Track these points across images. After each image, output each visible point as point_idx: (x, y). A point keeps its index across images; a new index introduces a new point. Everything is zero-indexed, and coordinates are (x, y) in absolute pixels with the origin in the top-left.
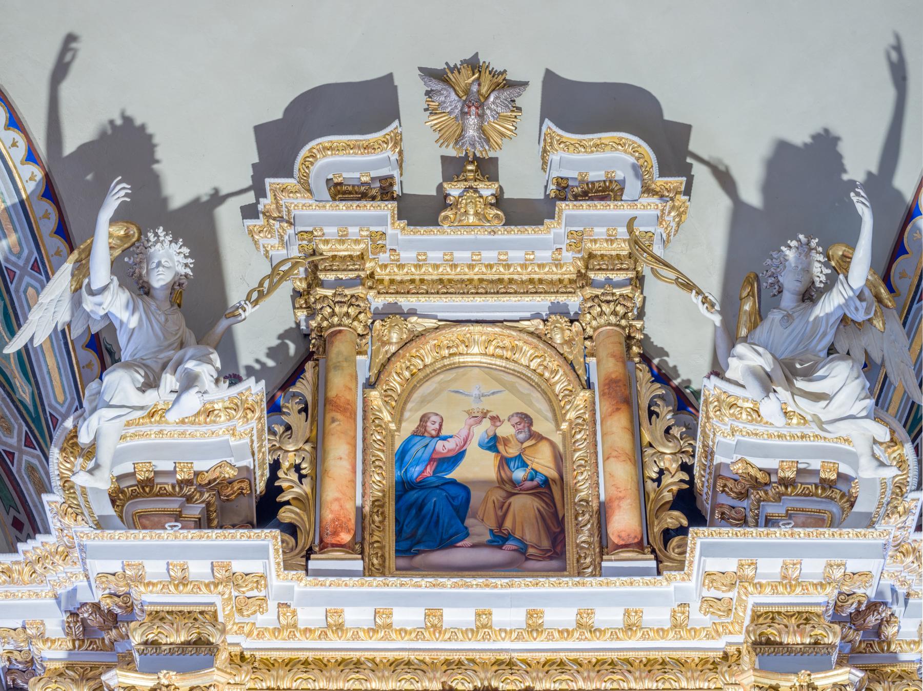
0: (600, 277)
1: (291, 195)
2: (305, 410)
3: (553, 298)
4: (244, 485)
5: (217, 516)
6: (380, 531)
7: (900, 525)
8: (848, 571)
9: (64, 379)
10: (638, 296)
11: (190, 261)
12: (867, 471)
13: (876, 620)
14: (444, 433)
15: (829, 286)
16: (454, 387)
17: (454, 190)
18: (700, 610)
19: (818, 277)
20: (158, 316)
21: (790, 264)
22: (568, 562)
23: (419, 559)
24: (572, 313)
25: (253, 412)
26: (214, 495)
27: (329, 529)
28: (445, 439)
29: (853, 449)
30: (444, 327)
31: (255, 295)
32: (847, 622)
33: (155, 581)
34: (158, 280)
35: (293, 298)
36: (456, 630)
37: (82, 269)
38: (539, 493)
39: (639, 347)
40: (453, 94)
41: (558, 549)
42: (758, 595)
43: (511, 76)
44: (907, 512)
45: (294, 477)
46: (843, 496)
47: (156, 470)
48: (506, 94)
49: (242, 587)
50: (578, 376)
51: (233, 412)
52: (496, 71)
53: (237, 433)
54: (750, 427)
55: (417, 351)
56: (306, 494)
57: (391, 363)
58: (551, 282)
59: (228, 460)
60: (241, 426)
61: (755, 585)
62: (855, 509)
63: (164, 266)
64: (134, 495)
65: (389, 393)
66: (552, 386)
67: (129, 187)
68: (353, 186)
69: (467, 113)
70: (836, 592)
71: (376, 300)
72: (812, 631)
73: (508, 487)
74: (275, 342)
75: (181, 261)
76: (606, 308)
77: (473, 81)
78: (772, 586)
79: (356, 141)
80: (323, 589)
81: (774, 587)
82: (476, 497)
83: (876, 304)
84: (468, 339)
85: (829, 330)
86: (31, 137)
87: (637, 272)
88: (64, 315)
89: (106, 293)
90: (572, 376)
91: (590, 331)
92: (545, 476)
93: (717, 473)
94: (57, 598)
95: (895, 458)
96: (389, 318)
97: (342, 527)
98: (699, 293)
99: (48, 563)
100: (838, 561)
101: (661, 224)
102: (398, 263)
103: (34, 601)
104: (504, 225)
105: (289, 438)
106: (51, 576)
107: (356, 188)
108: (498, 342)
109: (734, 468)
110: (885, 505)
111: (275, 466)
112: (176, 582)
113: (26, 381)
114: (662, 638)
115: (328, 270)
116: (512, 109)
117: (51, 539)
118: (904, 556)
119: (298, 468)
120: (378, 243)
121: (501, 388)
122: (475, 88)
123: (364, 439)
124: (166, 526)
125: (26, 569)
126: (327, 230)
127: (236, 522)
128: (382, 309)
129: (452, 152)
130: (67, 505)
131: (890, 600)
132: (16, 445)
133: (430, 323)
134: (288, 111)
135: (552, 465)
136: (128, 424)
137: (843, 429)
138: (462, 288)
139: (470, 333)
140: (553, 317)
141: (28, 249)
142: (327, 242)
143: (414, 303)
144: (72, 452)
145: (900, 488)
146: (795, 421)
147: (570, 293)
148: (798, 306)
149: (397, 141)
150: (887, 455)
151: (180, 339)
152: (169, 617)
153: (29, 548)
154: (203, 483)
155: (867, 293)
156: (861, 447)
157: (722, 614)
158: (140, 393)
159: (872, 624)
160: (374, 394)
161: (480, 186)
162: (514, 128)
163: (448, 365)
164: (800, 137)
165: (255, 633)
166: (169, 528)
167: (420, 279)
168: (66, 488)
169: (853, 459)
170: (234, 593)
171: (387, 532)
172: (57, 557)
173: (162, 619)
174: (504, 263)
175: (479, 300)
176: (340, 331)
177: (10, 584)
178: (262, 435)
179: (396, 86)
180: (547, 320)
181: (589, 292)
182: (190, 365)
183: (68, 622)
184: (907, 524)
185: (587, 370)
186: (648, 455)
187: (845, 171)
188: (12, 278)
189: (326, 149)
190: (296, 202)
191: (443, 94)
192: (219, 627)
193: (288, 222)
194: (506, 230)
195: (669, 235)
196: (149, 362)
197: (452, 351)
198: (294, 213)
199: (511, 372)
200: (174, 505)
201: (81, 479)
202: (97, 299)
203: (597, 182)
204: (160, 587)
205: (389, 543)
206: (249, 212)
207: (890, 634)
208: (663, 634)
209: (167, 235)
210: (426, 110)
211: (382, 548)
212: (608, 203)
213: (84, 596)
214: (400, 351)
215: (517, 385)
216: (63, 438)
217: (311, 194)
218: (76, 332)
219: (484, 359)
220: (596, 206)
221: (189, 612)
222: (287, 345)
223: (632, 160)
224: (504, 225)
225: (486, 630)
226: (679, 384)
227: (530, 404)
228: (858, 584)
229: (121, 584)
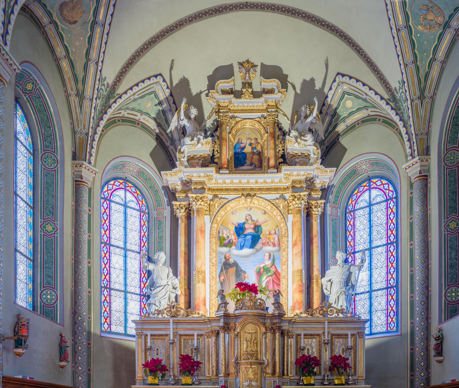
0: (270, 110)
2: (218, 138)
3: (262, 113)
11: (198, 112)
12: (312, 155)
14: (242, 142)
15: (310, 115)
16: (244, 132)
17: (244, 90)
23: (238, 168)
28: (242, 143)
43: (255, 64)
44: (318, 163)
45: (217, 153)
58: (261, 110)
64: (191, 159)
66: (261, 132)
74: (212, 122)
76: (271, 117)
88: (176, 124)
90: (265, 131)
93: (288, 153)
94: (179, 178)
98: (287, 117)
106: (178, 175)
111: (214, 150)
117: (178, 169)
122: (248, 68)
133: (240, 119)
134: (213, 72)
137: (309, 148)
141: (169, 107)
142: (221, 103)
153: (174, 170)
160: (230, 135)
164: (308, 79)
185: (267, 129)
187: (315, 87)
202: (182, 121)
227: (257, 136)
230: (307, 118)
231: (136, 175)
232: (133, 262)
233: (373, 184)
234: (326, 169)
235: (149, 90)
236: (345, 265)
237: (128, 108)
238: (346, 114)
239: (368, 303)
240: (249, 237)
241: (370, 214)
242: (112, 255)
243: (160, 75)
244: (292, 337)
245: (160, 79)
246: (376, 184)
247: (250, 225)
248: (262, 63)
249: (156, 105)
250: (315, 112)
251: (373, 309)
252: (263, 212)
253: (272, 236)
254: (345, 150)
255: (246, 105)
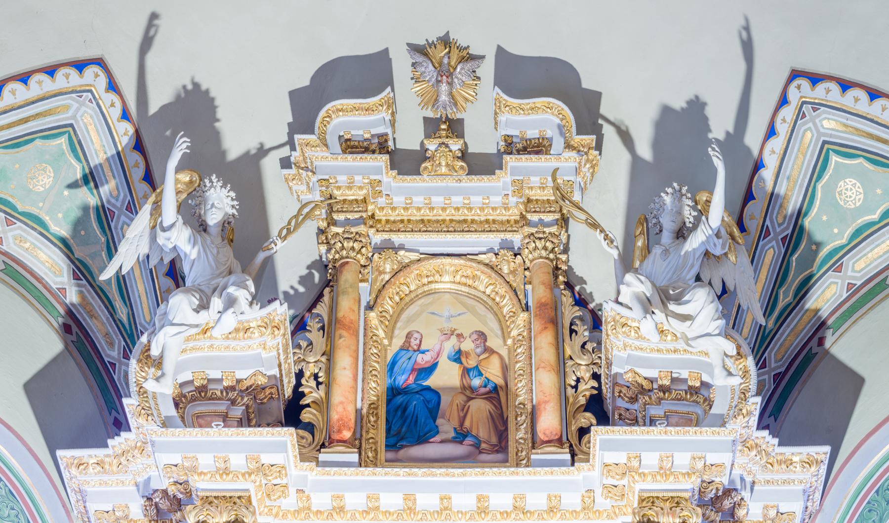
0: (534, 218)
1: (313, 149)
2: (323, 328)
3: (502, 236)
4: (274, 390)
5: (255, 417)
6: (374, 429)
7: (744, 425)
8: (708, 463)
9: (150, 302)
10: (564, 234)
11: (235, 203)
12: (719, 380)
13: (730, 503)
14: (423, 348)
15: (695, 226)
18: (602, 495)
19: (688, 218)
20: (211, 249)
21: (667, 209)
22: (510, 455)
23: (402, 453)
24: (516, 248)
25: (278, 329)
26: (251, 398)
27: (336, 428)
28: (423, 352)
29: (709, 360)
30: (424, 259)
31: (284, 232)
32: (709, 505)
33: (205, 471)
34: (212, 219)
35: (318, 235)
36: (426, 512)
37: (157, 208)
38: (490, 397)
39: (564, 277)
40: (431, 65)
41: (503, 444)
42: (642, 483)
44: (749, 413)
45: (313, 383)
46: (705, 400)
47: (209, 378)
48: (469, 65)
49: (268, 476)
50: (519, 300)
51: (264, 329)
52: (462, 46)
53: (267, 347)
54: (637, 343)
55: (404, 279)
56: (321, 398)
57: (385, 289)
58: (502, 223)
59: (260, 369)
60: (271, 342)
61: (640, 474)
62: (713, 411)
63: (216, 208)
64: (193, 399)
65: (384, 314)
67: (189, 140)
68: (359, 141)
69: (440, 81)
70: (699, 480)
71: (376, 236)
72: (681, 512)
73: (468, 393)
74: (304, 272)
75: (229, 203)
76: (540, 244)
77: (445, 55)
78: (652, 475)
79: (360, 104)
80: (329, 478)
81: (654, 476)
82: (445, 400)
83: (730, 241)
84: (441, 269)
85: (695, 262)
86: (125, 99)
87: (563, 215)
88: (144, 249)
89: (173, 229)
90: (515, 301)
91: (528, 264)
92: (496, 384)
94: (137, 485)
95: (741, 368)
96: (384, 252)
97: (344, 426)
98: (602, 231)
99: (130, 457)
100: (699, 454)
101: (579, 174)
102: (392, 206)
103: (120, 488)
104: (467, 175)
105: (310, 352)
106: (133, 467)
107: (361, 143)
108: (463, 272)
109: (626, 377)
110: (733, 408)
111: (300, 375)
112: (221, 472)
113: (123, 304)
114: (576, 519)
115: (340, 211)
116: (473, 78)
118: (749, 450)
119: (316, 377)
120: (376, 189)
121: (465, 310)
122: (446, 61)
123: (364, 352)
124: (213, 425)
125: (115, 461)
126: (339, 178)
127: (270, 421)
128: (380, 244)
129: (430, 114)
130: (141, 408)
131: (739, 487)
132: (116, 357)
133: (414, 256)
134: (313, 79)
135: (500, 374)
136: (188, 339)
137: (703, 344)
138: (438, 228)
139: (443, 265)
140: (502, 251)
141: (124, 192)
142: (339, 188)
143: (403, 239)
144: (146, 363)
145: (744, 393)
146: (669, 338)
147: (515, 231)
148: (673, 242)
149: (391, 104)
150: (735, 366)
151: (229, 268)
152: (216, 501)
153: (118, 443)
154: (243, 389)
155: (723, 232)
156: (715, 360)
157: (618, 498)
158: (195, 314)
159: (727, 507)
160: (372, 315)
161: (450, 142)
162: (475, 94)
163: (427, 291)
164: (678, 103)
165: (281, 514)
166: (215, 427)
167: (408, 220)
168: (141, 393)
169: (709, 368)
170: (264, 482)
171: (380, 430)
172: (136, 451)
173: (210, 503)
174: (468, 206)
175: (450, 237)
176: (347, 263)
177: (103, 474)
178: (288, 349)
179: (391, 59)
180: (498, 254)
181: (528, 230)
182: (231, 290)
183: (145, 505)
184: (750, 424)
185: (526, 296)
186: (569, 366)
187: (710, 131)
188: (112, 216)
189: (339, 110)
190: (316, 154)
191: (423, 66)
192: (251, 510)
193: (312, 171)
194: (468, 179)
195: (585, 183)
196: (203, 288)
197: (430, 279)
198: (315, 163)
199: (472, 297)
200: (222, 407)
201: (150, 386)
202: (167, 234)
203: (533, 139)
204: (209, 476)
205: (381, 439)
206: (286, 163)
207: (741, 515)
208: (576, 516)
209: (219, 181)
210: (412, 79)
211: (375, 443)
212: (540, 156)
213: (154, 485)
214: (392, 279)
215: (477, 308)
216: (140, 351)
217: (327, 148)
218: (153, 262)
219: (453, 286)
220: (532, 159)
221: (230, 497)
222: (313, 274)
223: (558, 121)
224: (467, 175)
225: (448, 512)
226: (594, 307)
227: (485, 324)
228: (715, 473)
229: (181, 474)
230: (685, 238)
234: (788, 450)
235: (48, 119)
238: (841, 234)
243: (99, 62)
245: (93, 77)
248: (500, 49)
249: (73, 186)
250: (717, 214)
254: (856, 382)
255: (437, 200)
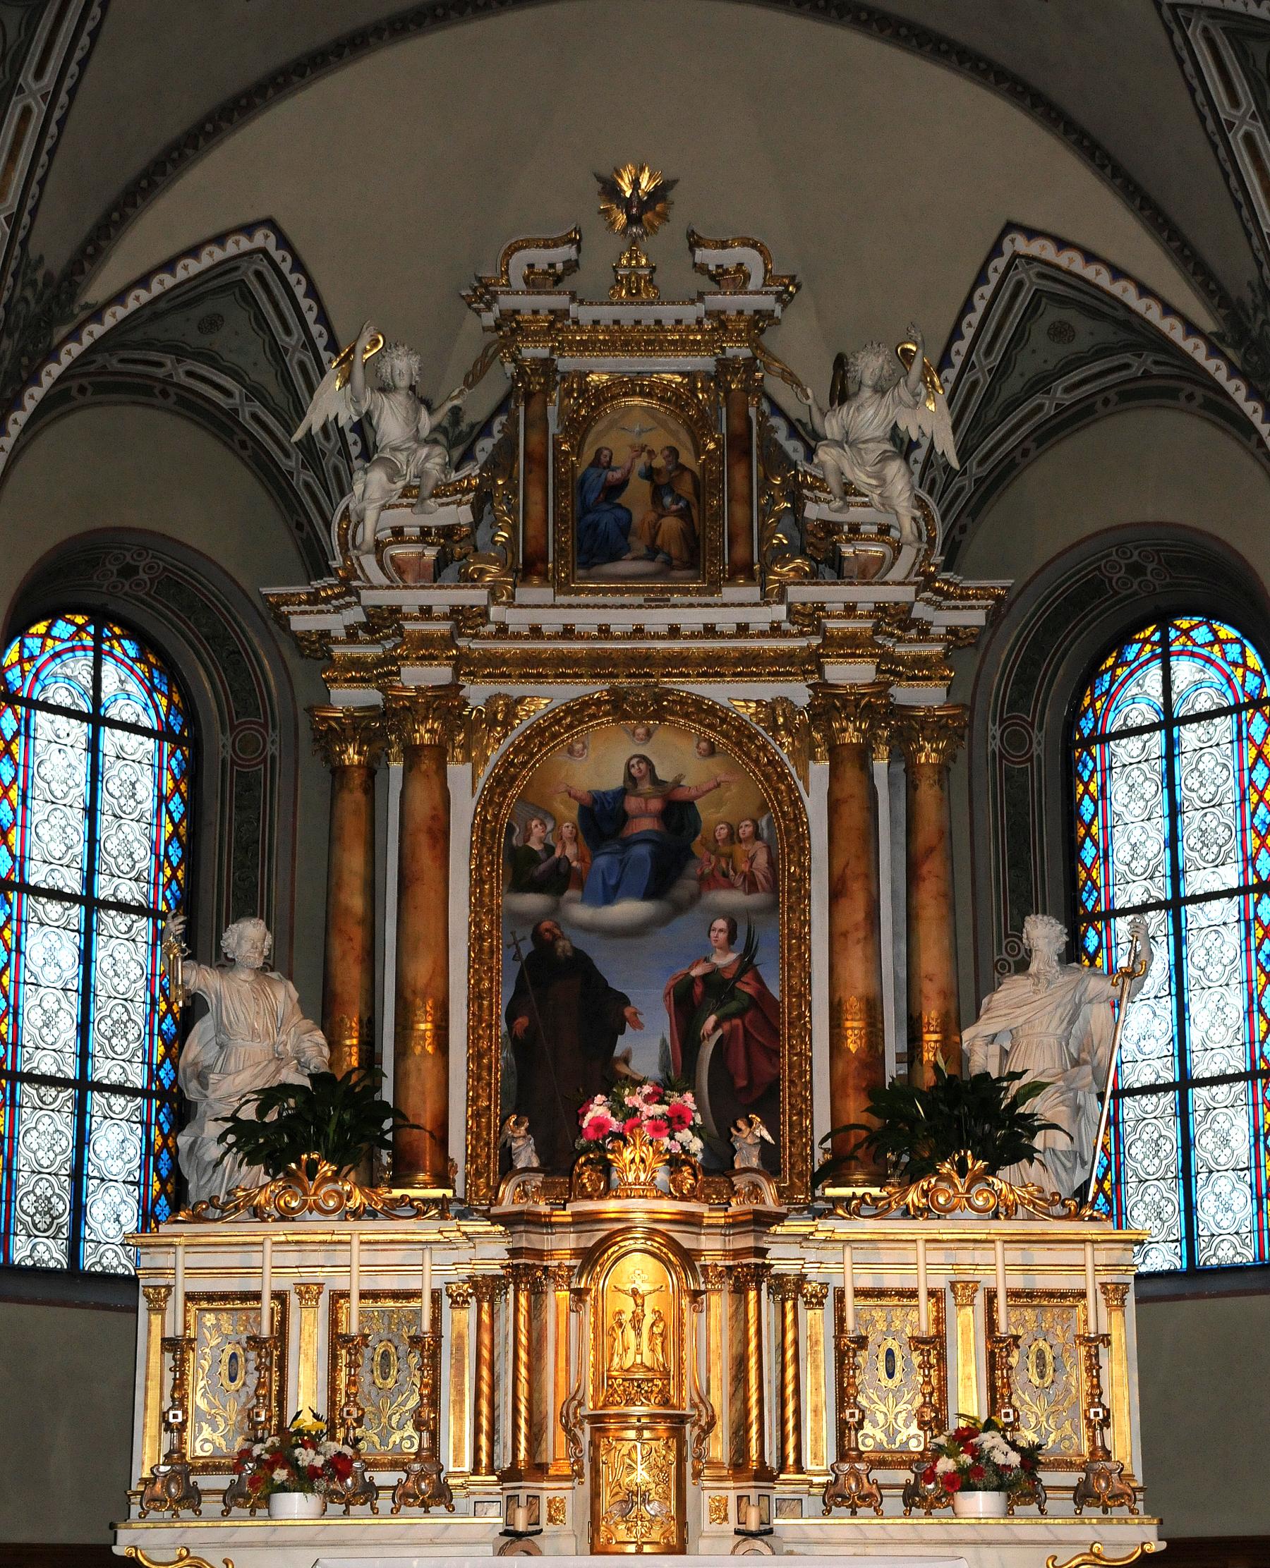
14: (613, 464)
23: (595, 570)
28: (614, 470)
231: (148, 594)
232: (123, 951)
233: (1177, 638)
236: (1063, 972)
237: (124, 346)
239: (1174, 1133)
240: (642, 850)
241: (1170, 756)
242: (30, 932)
244: (820, 1303)
246: (1190, 638)
247: (646, 800)
251: (1196, 1163)
252: (704, 745)
253: (744, 847)
